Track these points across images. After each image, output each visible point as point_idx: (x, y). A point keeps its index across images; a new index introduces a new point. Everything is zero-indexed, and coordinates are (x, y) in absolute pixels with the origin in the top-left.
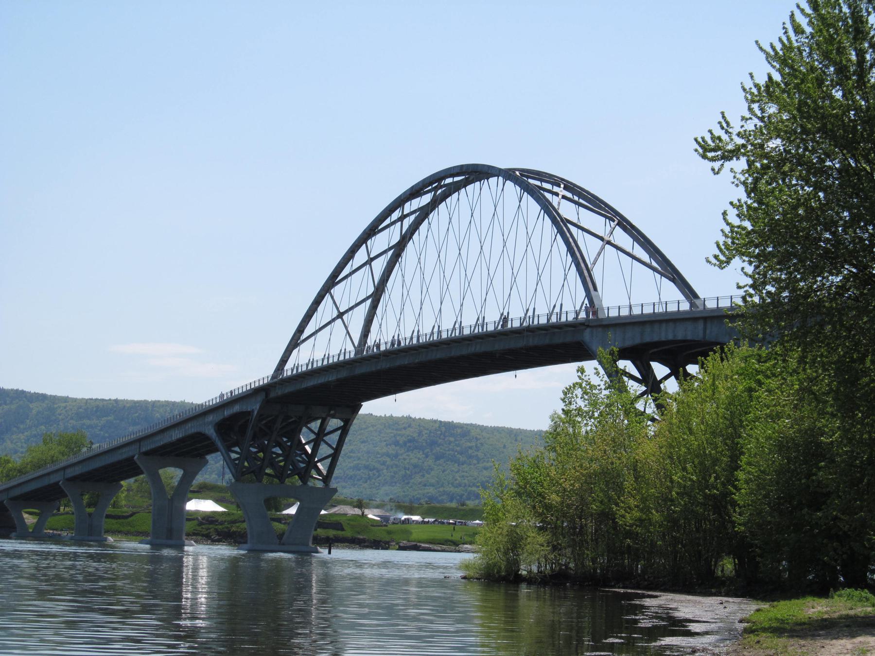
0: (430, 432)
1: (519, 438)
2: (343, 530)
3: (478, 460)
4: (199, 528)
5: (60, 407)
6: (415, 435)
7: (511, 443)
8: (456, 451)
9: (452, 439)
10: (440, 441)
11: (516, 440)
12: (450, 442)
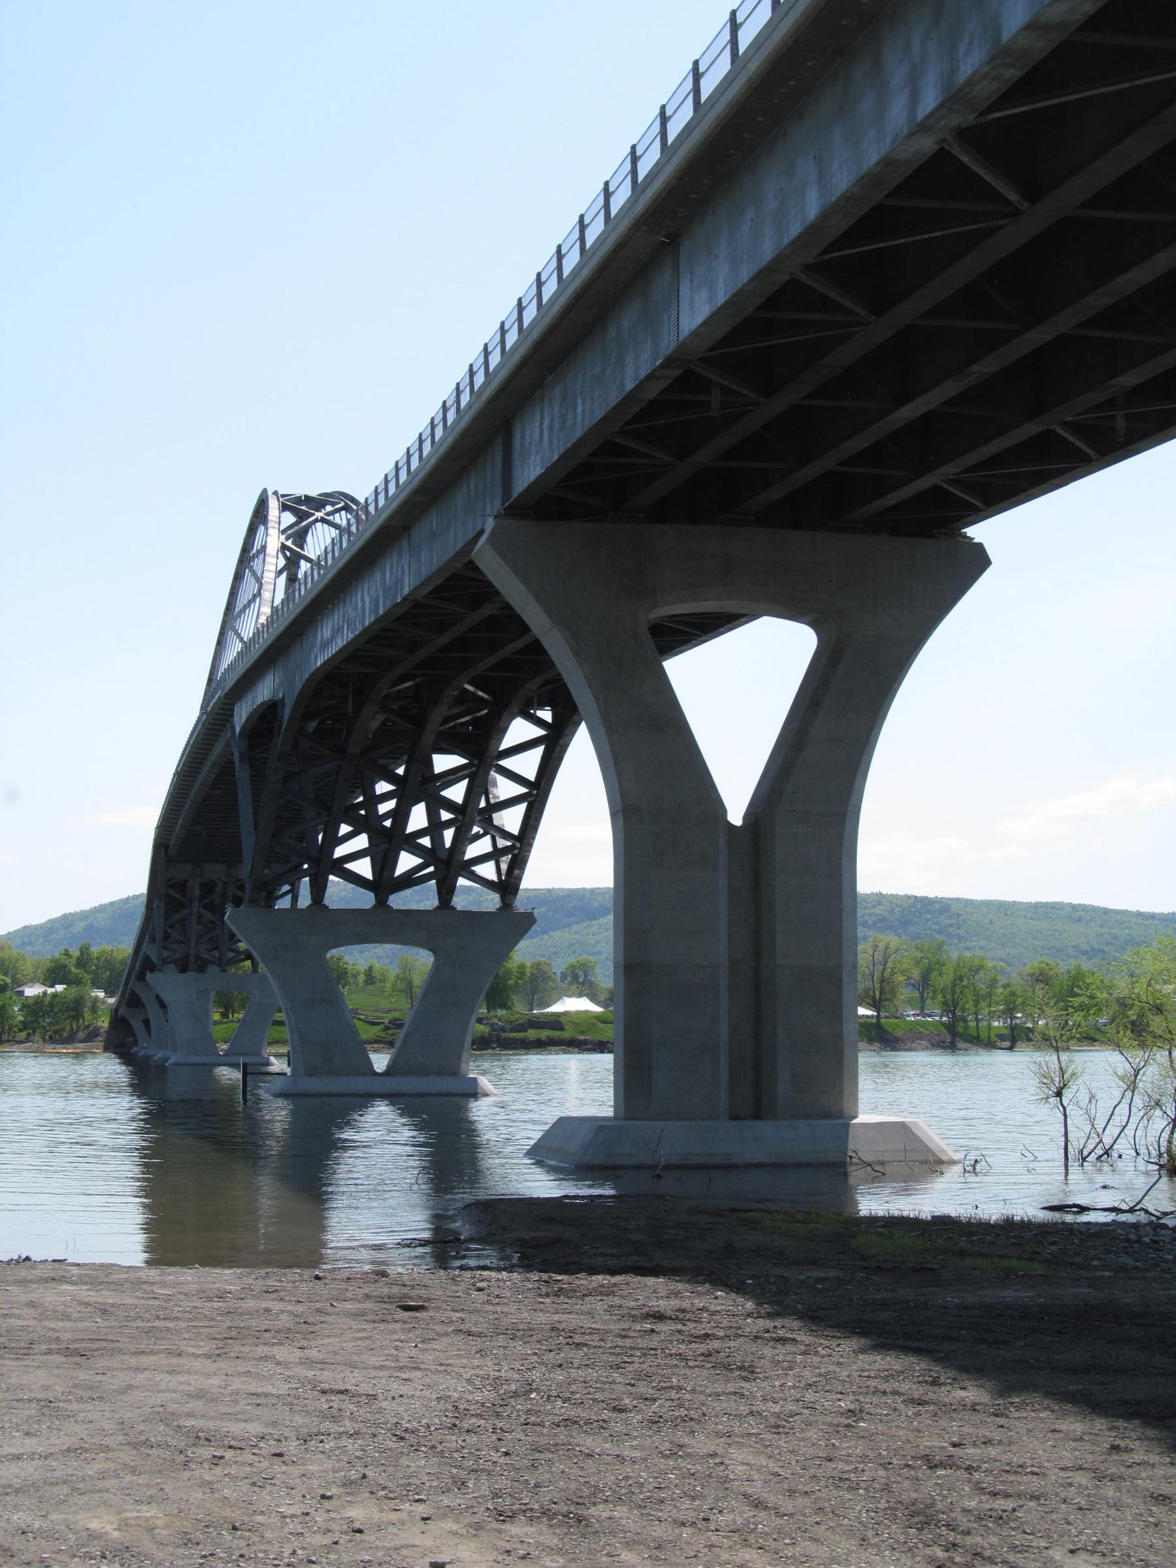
0: (904, 909)
1: (1009, 912)
2: (562, 1029)
3: (960, 939)
4: (383, 1034)
5: (487, 900)
6: (886, 914)
7: (999, 917)
8: (934, 930)
9: (929, 916)
10: (915, 919)
11: (1006, 915)
12: (927, 920)
